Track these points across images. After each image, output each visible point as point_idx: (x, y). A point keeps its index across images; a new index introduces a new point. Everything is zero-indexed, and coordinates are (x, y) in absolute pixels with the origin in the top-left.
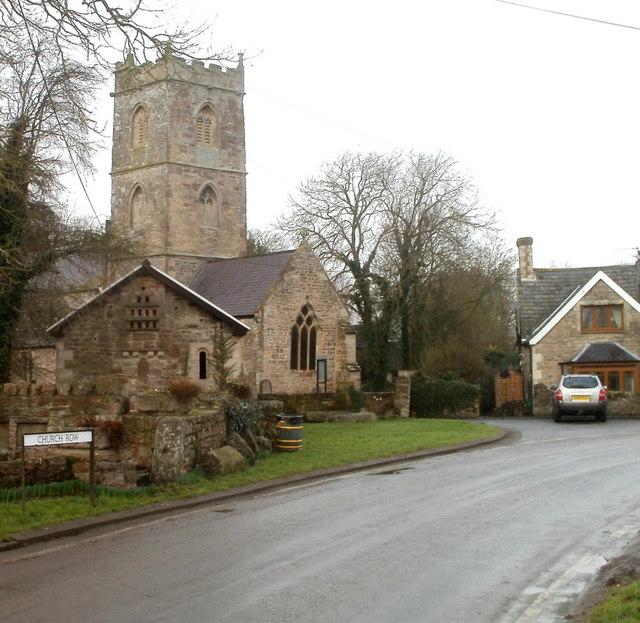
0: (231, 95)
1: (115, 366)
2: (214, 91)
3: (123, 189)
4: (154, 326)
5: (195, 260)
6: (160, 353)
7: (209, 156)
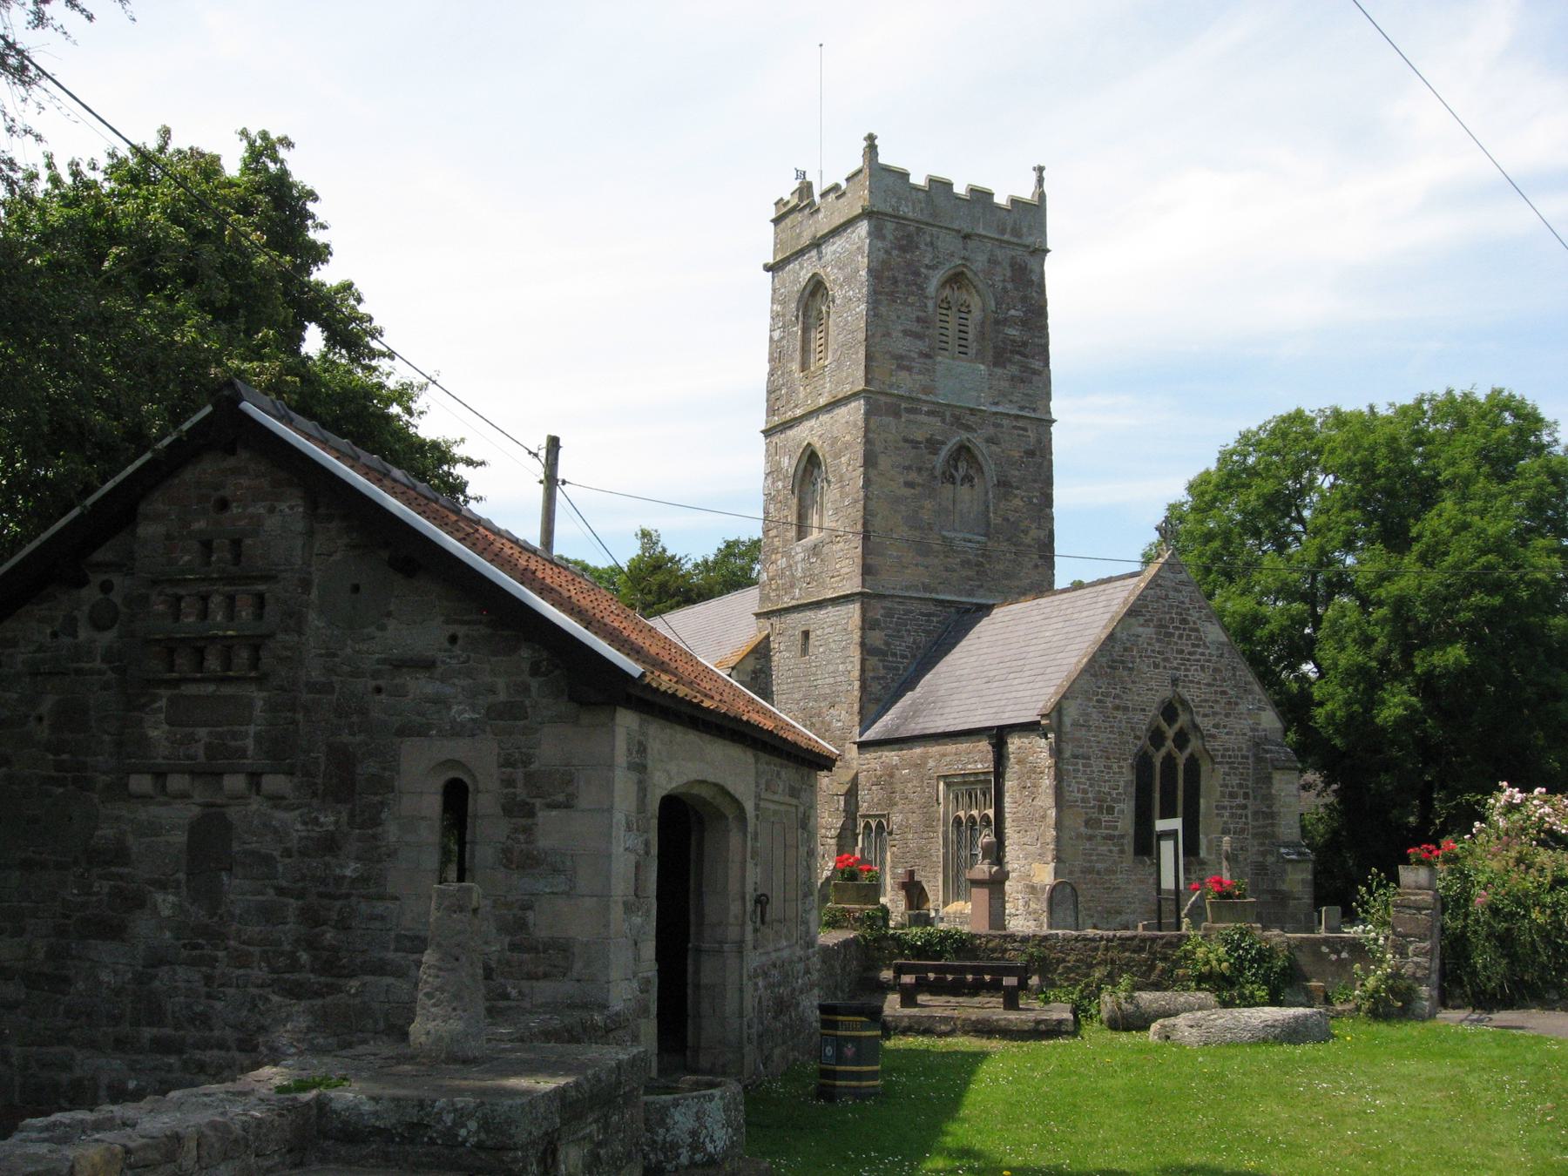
0: (1019, 252)
1: (106, 832)
3: (785, 462)
4: (255, 662)
5: (932, 608)
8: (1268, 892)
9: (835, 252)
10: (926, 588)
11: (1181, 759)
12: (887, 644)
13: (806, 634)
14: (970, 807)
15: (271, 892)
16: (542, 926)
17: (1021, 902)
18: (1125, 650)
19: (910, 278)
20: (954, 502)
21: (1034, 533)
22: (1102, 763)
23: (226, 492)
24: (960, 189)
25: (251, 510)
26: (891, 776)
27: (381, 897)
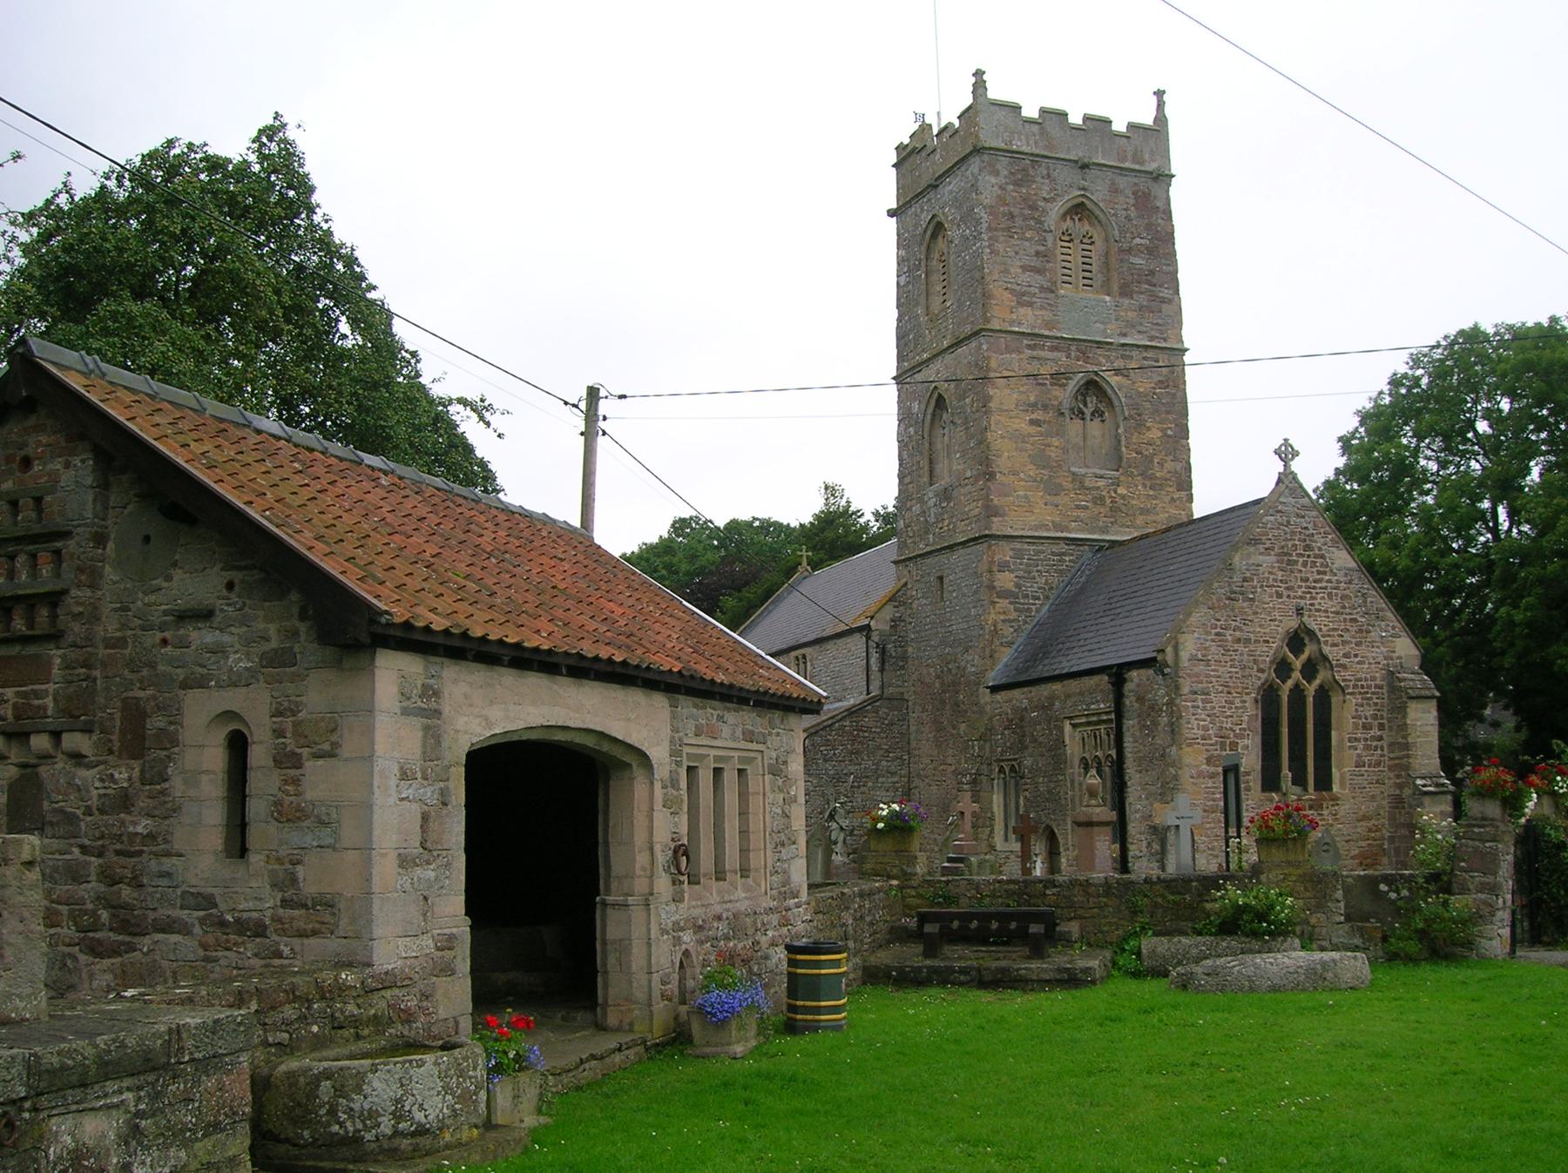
2: (1094, 172)
5: (1063, 547)
6: (72, 741)
7: (1092, 313)
8: (1403, 825)
9: (951, 192)
10: (1057, 527)
11: (1311, 689)
12: (1018, 586)
13: (941, 578)
14: (1096, 748)
15: (76, 850)
16: (311, 881)
17: (1144, 844)
18: (1245, 580)
19: (1027, 212)
20: (1085, 438)
21: (1169, 465)
22: (1223, 698)
23: (29, 451)
24: (1075, 119)
25: (50, 466)
26: (1022, 719)
27: (168, 854)
